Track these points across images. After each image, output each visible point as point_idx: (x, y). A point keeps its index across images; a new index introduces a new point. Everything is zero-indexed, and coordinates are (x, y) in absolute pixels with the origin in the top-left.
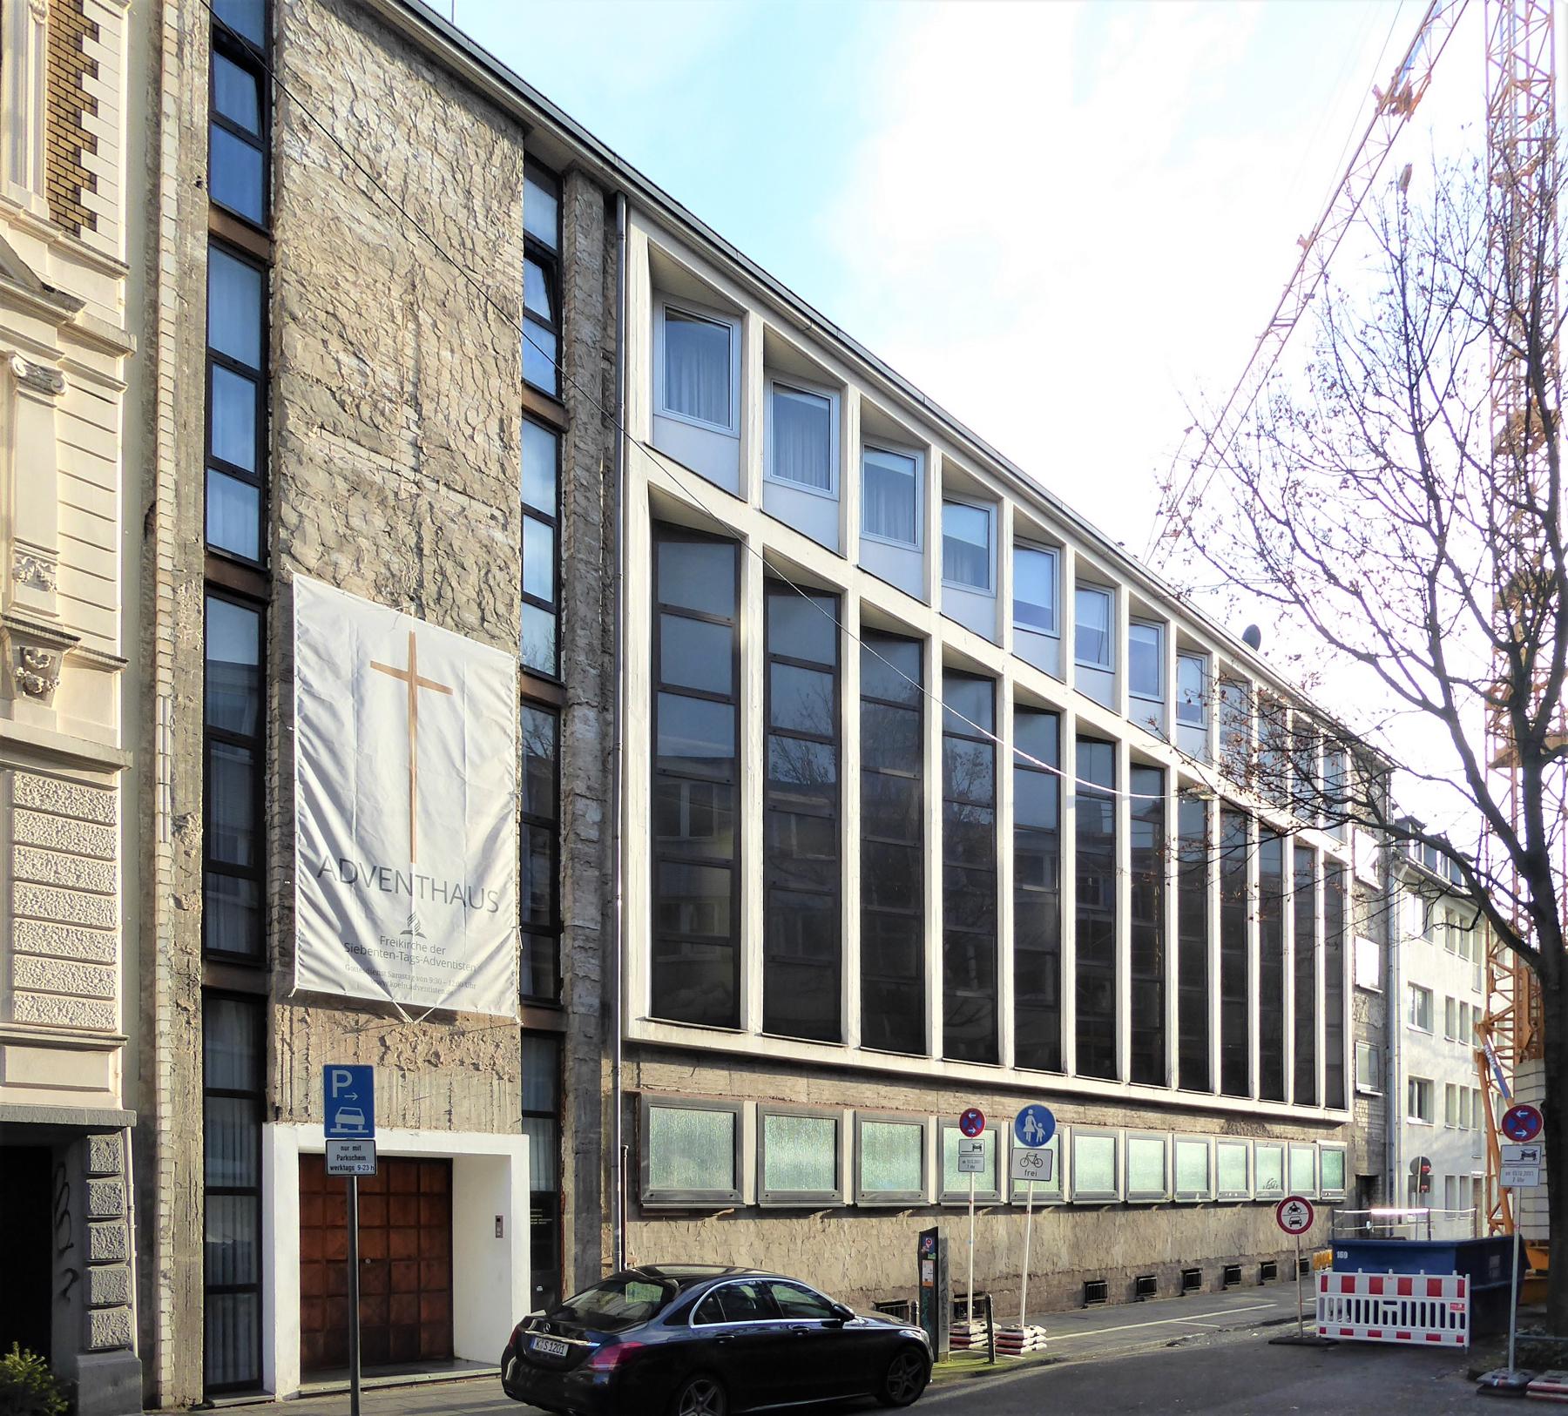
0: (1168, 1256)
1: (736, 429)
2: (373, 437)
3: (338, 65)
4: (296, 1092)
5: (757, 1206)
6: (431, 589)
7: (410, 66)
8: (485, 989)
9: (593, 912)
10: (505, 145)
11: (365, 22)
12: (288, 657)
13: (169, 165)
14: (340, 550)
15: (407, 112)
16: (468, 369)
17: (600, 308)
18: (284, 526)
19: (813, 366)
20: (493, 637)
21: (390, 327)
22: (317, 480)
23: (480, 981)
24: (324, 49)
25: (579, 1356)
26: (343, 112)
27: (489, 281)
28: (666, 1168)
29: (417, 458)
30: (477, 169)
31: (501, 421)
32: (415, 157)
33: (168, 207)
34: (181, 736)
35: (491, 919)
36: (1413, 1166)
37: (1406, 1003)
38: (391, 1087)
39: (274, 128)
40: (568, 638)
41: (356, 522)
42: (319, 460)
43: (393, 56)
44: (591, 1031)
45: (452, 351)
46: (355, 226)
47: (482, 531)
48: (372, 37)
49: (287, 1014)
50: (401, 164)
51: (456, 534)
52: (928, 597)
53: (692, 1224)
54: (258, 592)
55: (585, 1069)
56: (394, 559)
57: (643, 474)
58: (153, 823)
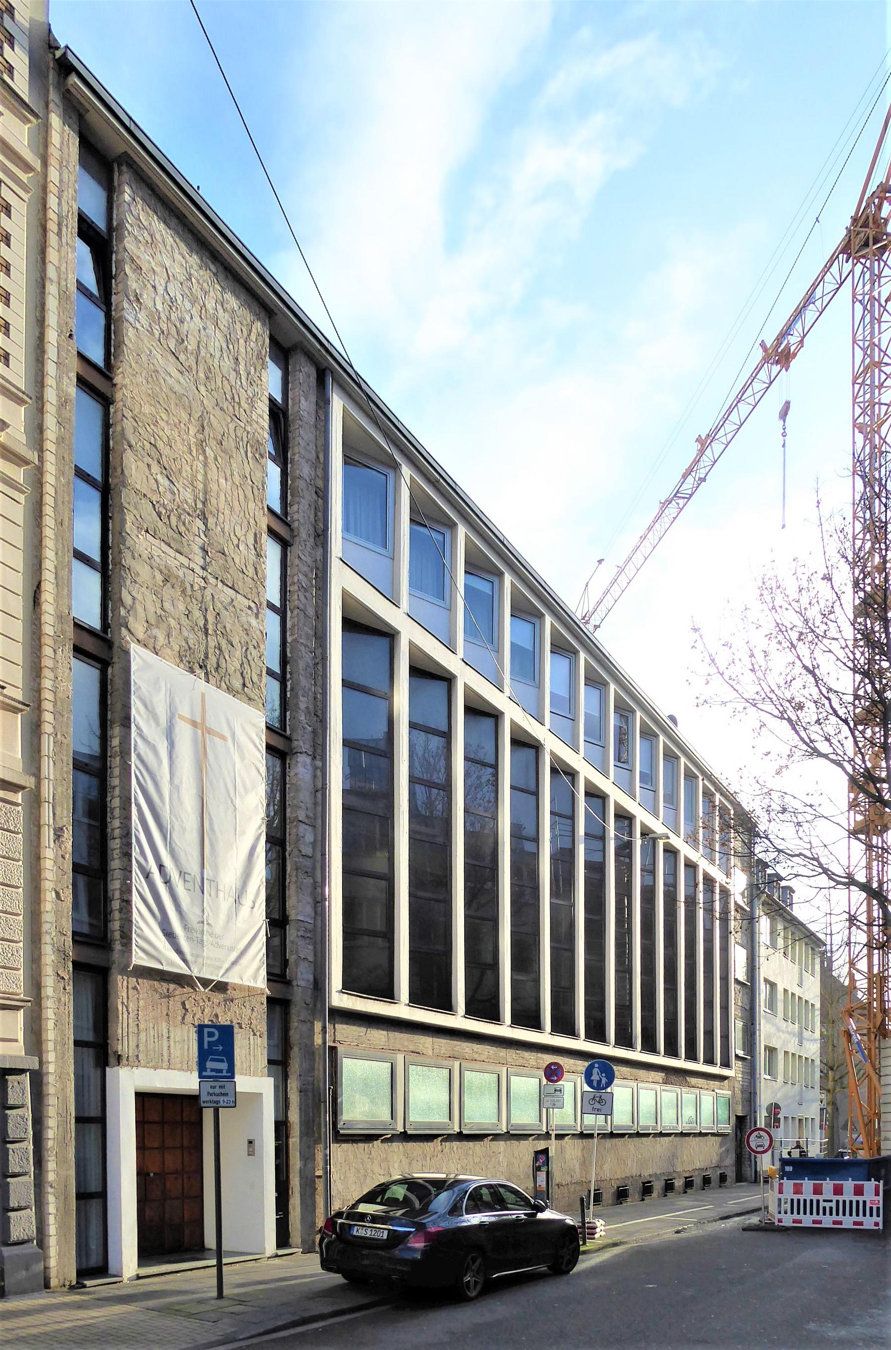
0: (635, 1172)
1: (391, 550)
3: (158, 253)
4: (131, 1043)
5: (405, 1132)
7: (202, 260)
9: (309, 910)
10: (258, 324)
11: (174, 222)
12: (127, 707)
13: (52, 319)
14: (158, 627)
15: (200, 294)
16: (235, 494)
19: (442, 508)
21: (189, 458)
22: (143, 571)
25: (396, 1239)
26: (160, 290)
27: (249, 428)
29: (205, 559)
30: (242, 341)
31: (255, 534)
32: (204, 329)
33: (51, 352)
36: (769, 1109)
37: (763, 992)
39: (114, 296)
40: (291, 703)
41: (167, 605)
42: (145, 556)
43: (191, 251)
44: (309, 1000)
45: (226, 479)
46: (168, 378)
47: (243, 619)
48: (178, 234)
49: (125, 982)
50: (196, 333)
51: (228, 619)
52: (503, 687)
53: (366, 1145)
54: (103, 656)
57: (342, 581)
58: (39, 832)
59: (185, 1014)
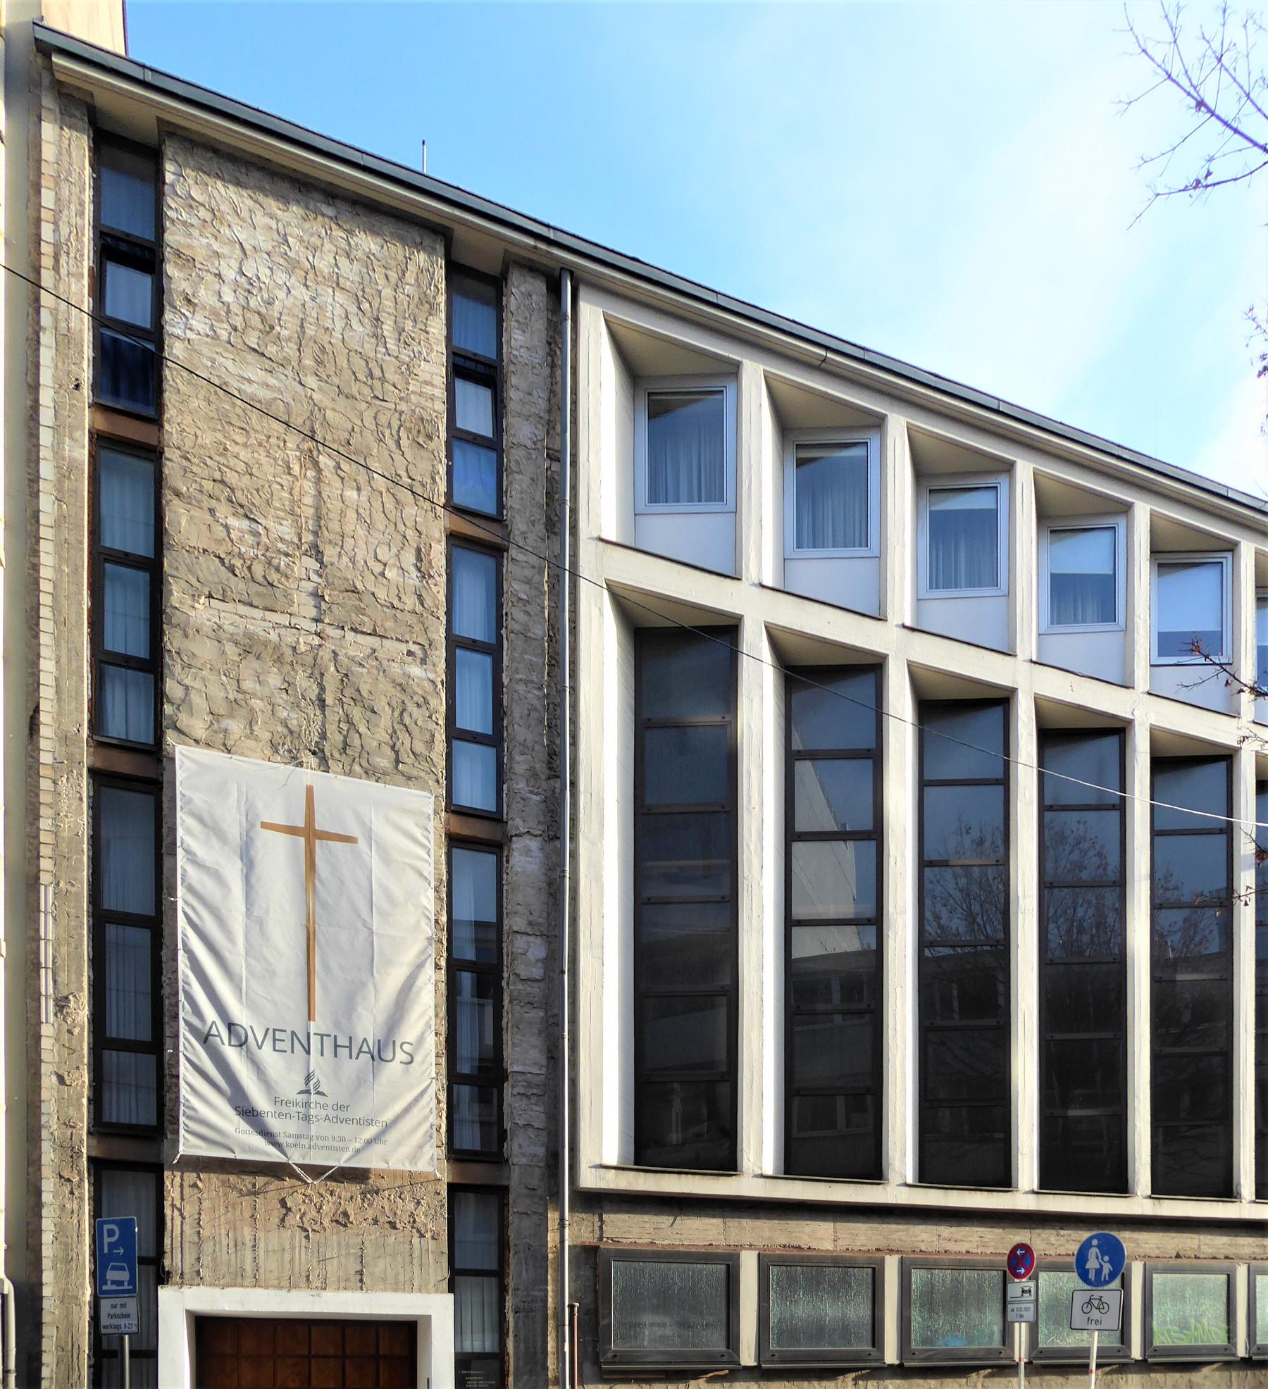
2: (267, 592)
3: (224, 230)
4: (187, 1256)
6: (335, 738)
8: (399, 1143)
14: (231, 716)
17: (542, 404)
18: (169, 702)
20: (409, 778)
21: (285, 480)
22: (204, 650)
23: (392, 1137)
24: (208, 216)
26: (230, 274)
27: (403, 407)
28: (634, 1328)
29: (318, 607)
30: (387, 292)
31: (419, 550)
34: (64, 921)
35: (406, 1072)
38: (293, 1248)
41: (248, 685)
42: (207, 630)
44: (535, 1182)
45: (359, 489)
48: (261, 189)
49: (178, 1180)
51: (365, 680)
55: (526, 1223)
56: (293, 715)
59: (285, 1215)
